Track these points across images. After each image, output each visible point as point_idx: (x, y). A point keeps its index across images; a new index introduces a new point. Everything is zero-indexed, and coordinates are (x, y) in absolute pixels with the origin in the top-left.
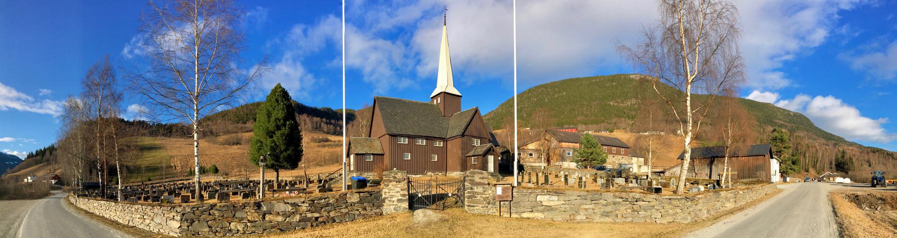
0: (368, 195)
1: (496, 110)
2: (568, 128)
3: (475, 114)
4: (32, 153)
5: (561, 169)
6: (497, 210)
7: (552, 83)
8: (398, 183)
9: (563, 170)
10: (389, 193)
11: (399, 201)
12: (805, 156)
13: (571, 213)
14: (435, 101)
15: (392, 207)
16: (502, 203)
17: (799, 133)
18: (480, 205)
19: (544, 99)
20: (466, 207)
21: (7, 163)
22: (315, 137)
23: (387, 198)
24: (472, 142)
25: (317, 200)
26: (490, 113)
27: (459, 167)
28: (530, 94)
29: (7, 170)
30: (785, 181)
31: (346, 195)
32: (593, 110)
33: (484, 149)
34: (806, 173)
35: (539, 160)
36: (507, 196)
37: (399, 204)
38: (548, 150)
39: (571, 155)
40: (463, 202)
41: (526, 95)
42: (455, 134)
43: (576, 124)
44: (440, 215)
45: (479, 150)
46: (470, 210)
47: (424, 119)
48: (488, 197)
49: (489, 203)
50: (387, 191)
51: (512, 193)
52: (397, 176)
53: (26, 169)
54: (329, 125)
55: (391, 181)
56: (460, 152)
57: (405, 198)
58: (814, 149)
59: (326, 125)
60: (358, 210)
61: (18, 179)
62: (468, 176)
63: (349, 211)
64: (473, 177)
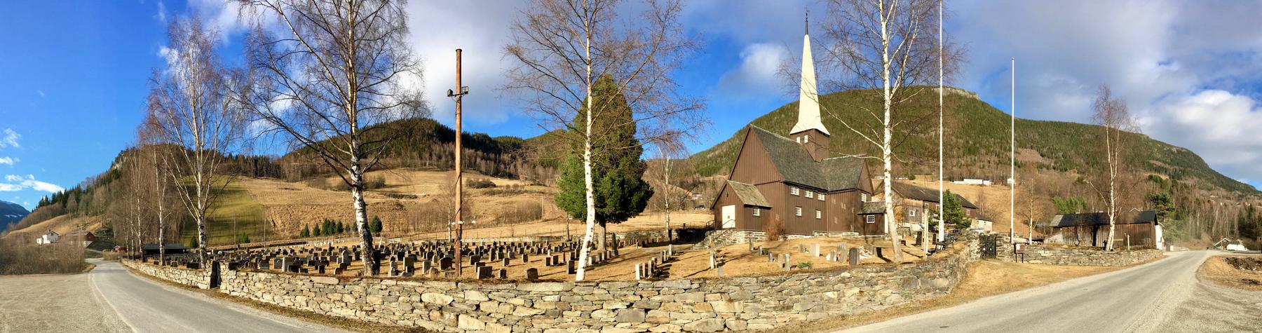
4: (47, 198)
12: (1194, 217)
17: (1186, 180)
21: (8, 216)
22: (472, 179)
26: (719, 146)
28: (783, 116)
29: (9, 224)
30: (1168, 250)
34: (1197, 240)
41: (776, 118)
53: (37, 223)
54: (488, 162)
58: (1208, 206)
59: (484, 162)
61: (28, 238)
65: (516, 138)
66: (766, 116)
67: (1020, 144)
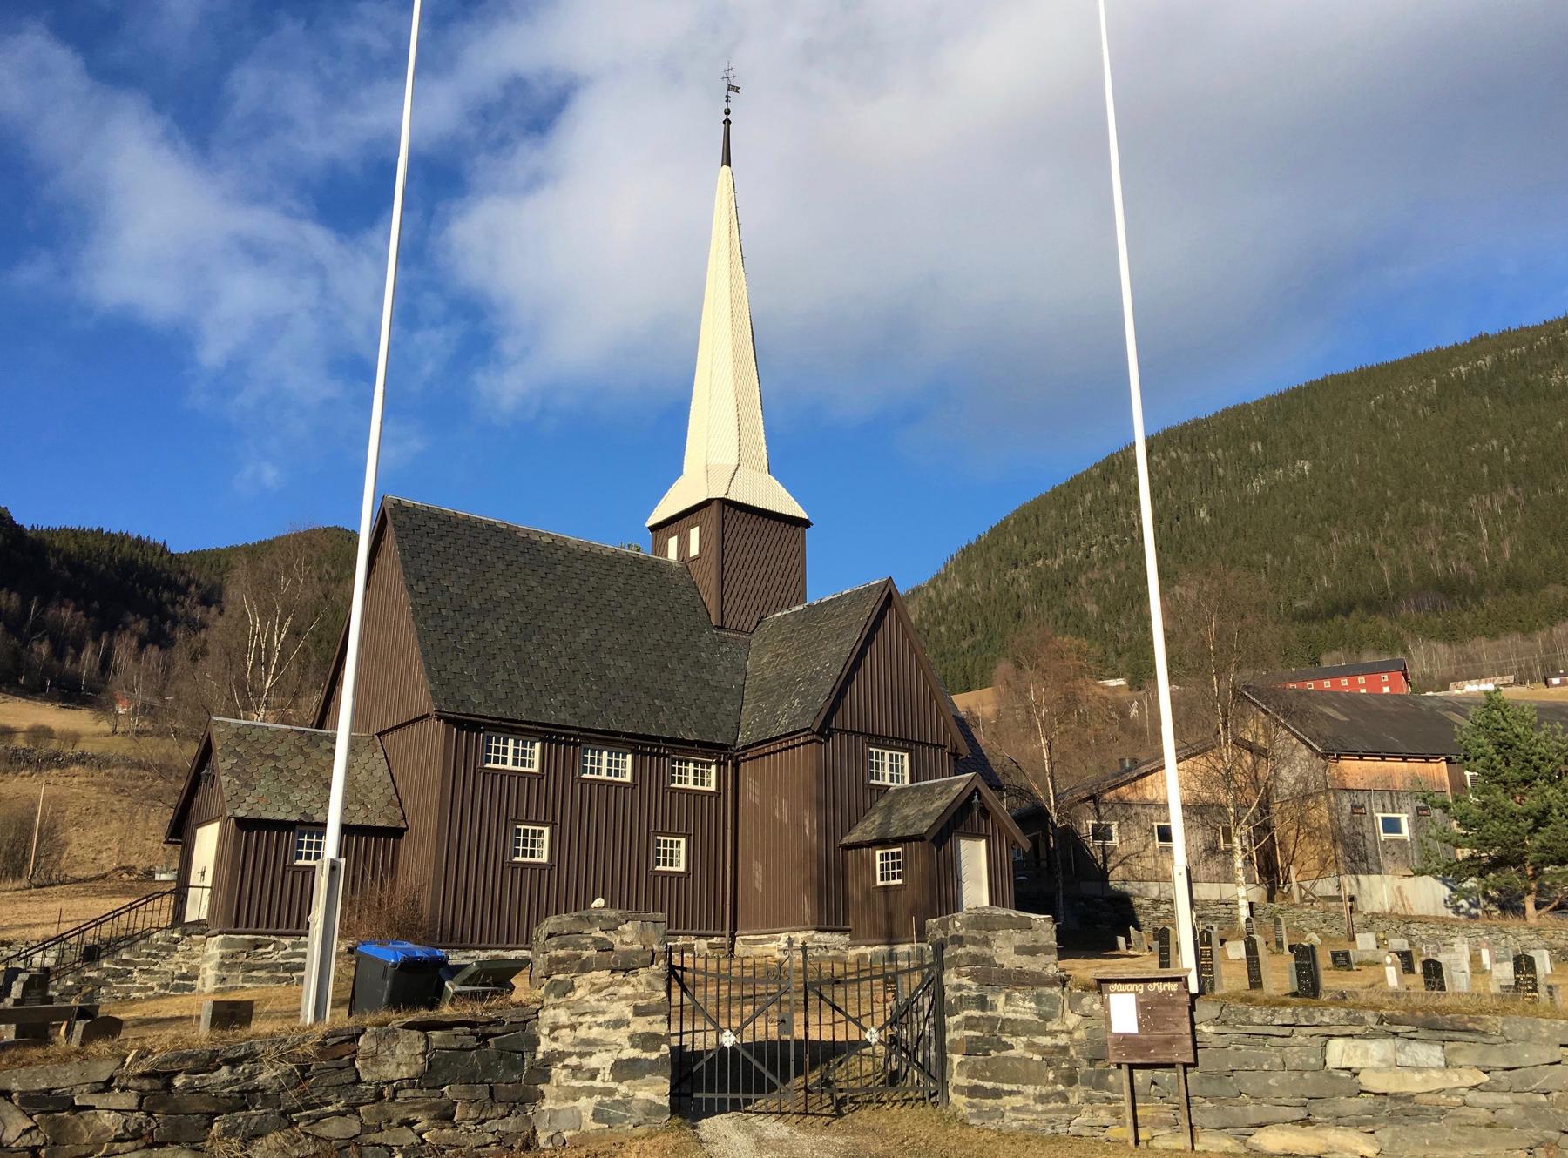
0: (472, 1042)
1: (932, 583)
2: (1351, 671)
3: (881, 616)
5: (1357, 919)
6: (1116, 1113)
7: (1225, 412)
8: (619, 976)
9: (1368, 926)
10: (573, 1027)
11: (624, 1069)
13: (1534, 1133)
14: (673, 543)
15: (586, 1104)
16: (1139, 1075)
18: (1030, 1090)
19: (1190, 509)
20: (958, 1101)
23: (562, 1056)
24: (866, 766)
25: (189, 1072)
27: (807, 909)
28: (1114, 487)
31: (354, 1039)
32: (1484, 546)
33: (939, 804)
35: (1215, 866)
36: (1169, 1043)
37: (623, 1088)
38: (1265, 806)
39: (1406, 833)
40: (937, 1073)
41: (1089, 496)
42: (783, 725)
43: (1396, 643)
44: (839, 1141)
45: (907, 811)
46: (980, 1114)
47: (624, 639)
48: (1065, 1049)
49: (1071, 1080)
50: (563, 1016)
51: (1193, 1024)
52: (615, 939)
55: (585, 967)
56: (809, 823)
57: (654, 1056)
60: (410, 1124)
62: (959, 941)
63: (366, 1129)
64: (986, 942)
65: (139, 542)
66: (1056, 492)
67: (1385, 832)
